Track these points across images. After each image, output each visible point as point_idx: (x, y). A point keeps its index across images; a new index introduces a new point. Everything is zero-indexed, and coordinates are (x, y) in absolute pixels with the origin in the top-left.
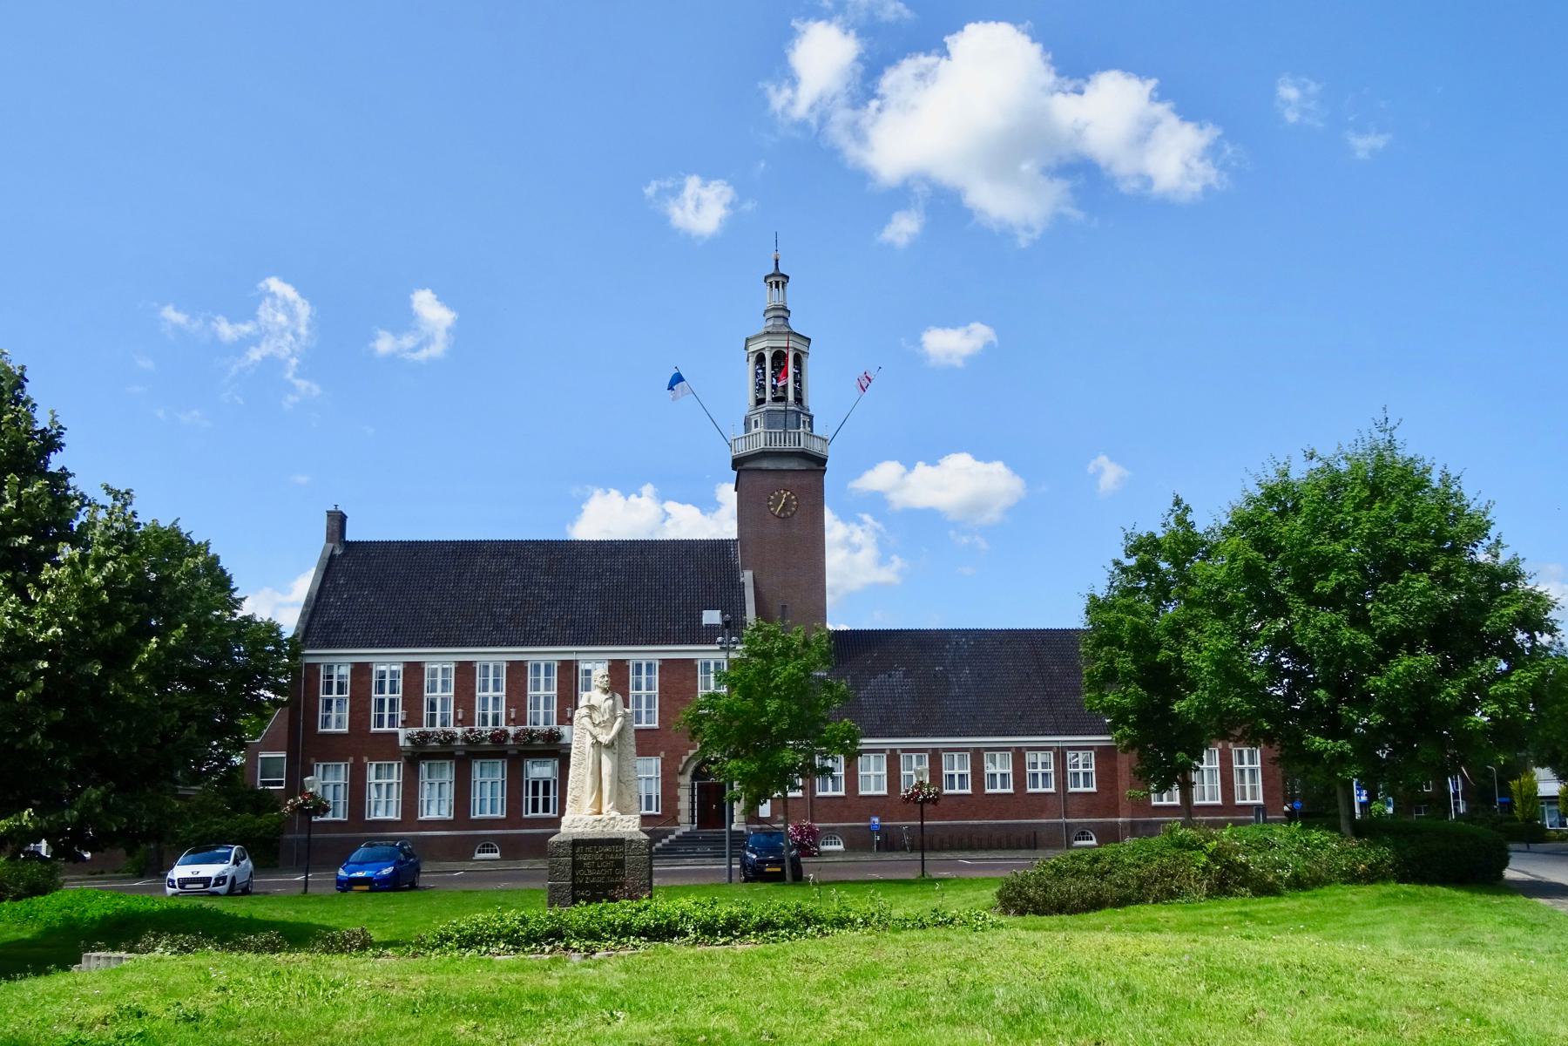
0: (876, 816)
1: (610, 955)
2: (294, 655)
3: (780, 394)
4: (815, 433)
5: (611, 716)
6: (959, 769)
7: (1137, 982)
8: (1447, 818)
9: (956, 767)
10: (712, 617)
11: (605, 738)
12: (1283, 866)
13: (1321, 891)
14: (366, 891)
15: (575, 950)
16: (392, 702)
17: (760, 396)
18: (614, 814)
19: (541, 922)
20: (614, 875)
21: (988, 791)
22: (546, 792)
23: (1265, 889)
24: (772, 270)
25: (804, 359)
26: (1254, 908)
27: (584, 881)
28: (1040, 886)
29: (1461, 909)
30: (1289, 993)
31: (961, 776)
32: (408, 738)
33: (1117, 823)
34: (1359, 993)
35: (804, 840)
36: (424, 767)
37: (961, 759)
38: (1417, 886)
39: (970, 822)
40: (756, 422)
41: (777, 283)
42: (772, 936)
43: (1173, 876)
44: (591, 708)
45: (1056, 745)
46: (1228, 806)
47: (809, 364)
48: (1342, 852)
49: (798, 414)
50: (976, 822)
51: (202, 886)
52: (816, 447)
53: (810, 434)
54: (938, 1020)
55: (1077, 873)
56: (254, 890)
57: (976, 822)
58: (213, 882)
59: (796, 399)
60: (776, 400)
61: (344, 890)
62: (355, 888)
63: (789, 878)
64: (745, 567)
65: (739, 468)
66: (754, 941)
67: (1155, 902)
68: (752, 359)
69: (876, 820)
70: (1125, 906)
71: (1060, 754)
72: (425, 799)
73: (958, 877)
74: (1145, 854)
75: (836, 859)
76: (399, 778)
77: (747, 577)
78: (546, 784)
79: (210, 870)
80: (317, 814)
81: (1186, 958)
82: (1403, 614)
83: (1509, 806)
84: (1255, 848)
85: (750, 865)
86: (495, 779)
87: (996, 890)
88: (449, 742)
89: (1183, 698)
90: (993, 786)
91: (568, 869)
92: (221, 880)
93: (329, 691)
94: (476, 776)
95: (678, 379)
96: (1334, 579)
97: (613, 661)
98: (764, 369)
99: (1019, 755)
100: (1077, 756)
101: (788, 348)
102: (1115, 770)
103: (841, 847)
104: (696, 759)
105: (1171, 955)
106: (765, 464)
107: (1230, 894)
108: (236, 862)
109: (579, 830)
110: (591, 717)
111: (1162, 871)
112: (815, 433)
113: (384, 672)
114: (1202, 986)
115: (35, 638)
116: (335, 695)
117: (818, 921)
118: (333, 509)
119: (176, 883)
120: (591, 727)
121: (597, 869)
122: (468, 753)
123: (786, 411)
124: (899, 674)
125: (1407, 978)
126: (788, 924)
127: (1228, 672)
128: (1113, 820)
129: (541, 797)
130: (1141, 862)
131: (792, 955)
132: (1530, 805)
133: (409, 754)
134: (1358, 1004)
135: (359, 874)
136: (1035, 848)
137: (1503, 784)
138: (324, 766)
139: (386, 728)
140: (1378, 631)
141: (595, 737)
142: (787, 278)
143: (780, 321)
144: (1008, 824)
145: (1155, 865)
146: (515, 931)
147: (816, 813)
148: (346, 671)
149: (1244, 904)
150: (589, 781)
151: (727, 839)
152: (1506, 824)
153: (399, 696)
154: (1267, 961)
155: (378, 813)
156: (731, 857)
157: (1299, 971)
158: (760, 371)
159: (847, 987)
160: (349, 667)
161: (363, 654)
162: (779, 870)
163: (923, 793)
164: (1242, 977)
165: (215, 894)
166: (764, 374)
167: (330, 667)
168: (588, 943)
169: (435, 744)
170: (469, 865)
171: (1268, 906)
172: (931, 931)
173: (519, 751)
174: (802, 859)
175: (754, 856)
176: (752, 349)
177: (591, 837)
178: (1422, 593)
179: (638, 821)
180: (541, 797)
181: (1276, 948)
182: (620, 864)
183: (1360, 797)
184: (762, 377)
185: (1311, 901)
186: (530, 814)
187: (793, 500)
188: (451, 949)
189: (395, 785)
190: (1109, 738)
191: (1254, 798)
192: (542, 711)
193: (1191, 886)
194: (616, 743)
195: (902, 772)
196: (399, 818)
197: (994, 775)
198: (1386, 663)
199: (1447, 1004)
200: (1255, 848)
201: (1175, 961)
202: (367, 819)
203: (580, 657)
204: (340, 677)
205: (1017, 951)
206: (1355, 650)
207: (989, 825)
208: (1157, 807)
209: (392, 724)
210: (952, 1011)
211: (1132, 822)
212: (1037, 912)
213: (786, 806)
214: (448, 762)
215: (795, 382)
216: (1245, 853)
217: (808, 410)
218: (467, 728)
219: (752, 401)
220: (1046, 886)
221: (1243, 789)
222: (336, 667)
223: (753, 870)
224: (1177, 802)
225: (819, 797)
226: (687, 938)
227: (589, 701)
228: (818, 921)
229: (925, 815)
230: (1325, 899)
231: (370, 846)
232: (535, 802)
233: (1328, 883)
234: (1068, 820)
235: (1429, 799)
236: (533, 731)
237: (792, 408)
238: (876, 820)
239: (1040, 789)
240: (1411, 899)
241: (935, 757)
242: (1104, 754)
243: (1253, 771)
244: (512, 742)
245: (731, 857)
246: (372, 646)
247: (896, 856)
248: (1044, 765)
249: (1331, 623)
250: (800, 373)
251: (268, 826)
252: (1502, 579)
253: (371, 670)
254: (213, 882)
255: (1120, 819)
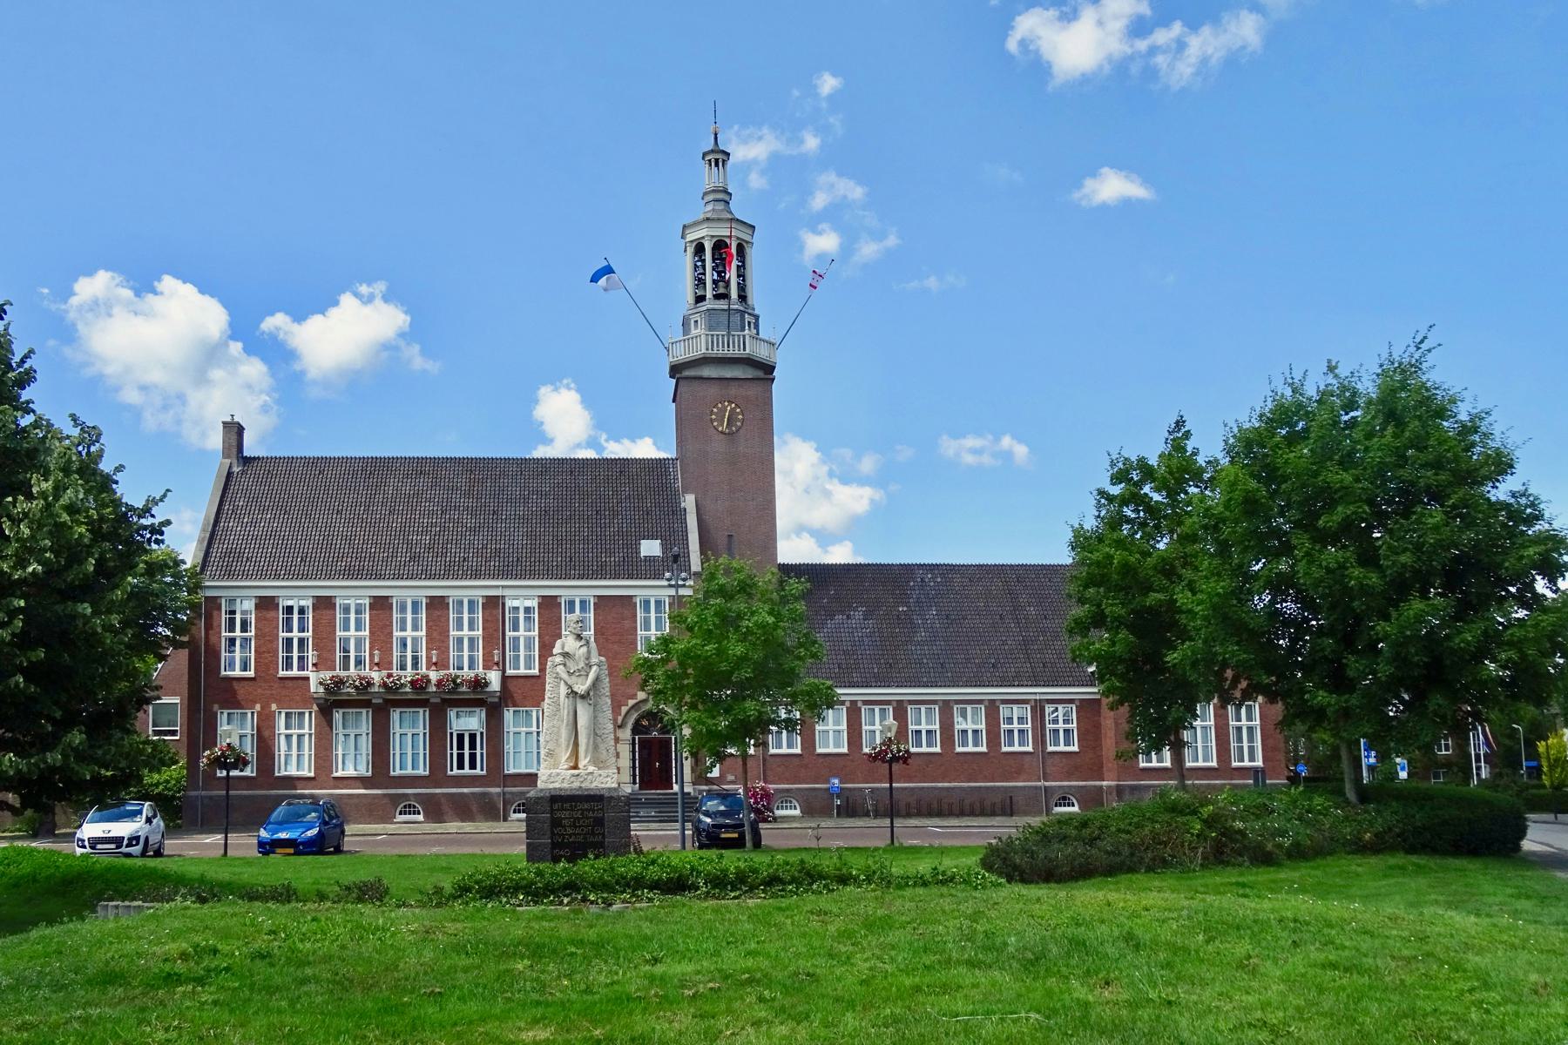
0: (835, 776)
1: (627, 907)
2: (195, 588)
3: (722, 290)
4: (761, 336)
5: (587, 665)
6: (927, 724)
7: (1139, 932)
8: (1469, 785)
9: (925, 722)
10: (651, 548)
11: (581, 688)
12: (1283, 833)
13: (1324, 862)
14: (289, 854)
15: (592, 902)
16: (301, 641)
17: (700, 293)
18: (591, 769)
19: (558, 875)
20: (593, 834)
21: (959, 749)
22: (473, 746)
23: (1264, 858)
24: (711, 146)
25: (748, 250)
26: (1252, 878)
27: (564, 838)
28: (1027, 852)
29: (1472, 881)
30: (1282, 942)
31: (929, 732)
32: (321, 683)
33: (1101, 787)
34: (1347, 944)
35: (758, 803)
36: (338, 716)
37: (929, 711)
38: (1427, 858)
39: (940, 785)
40: (696, 322)
41: (717, 161)
42: (780, 890)
43: (1165, 844)
44: (566, 655)
45: (1033, 697)
46: (1224, 770)
47: (753, 255)
48: (1346, 818)
49: (742, 313)
50: (946, 785)
51: (113, 846)
52: (762, 352)
53: (756, 337)
54: (958, 962)
55: (1064, 839)
56: (165, 853)
57: (946, 785)
58: (125, 842)
59: (740, 296)
60: (717, 297)
61: (265, 853)
62: (278, 850)
63: (749, 844)
64: (686, 490)
65: (678, 376)
66: (763, 895)
67: (1146, 872)
68: (691, 250)
69: (836, 781)
70: (1116, 875)
71: (1038, 708)
72: (340, 752)
73: (931, 846)
74: (1135, 820)
75: (794, 825)
76: (310, 729)
77: (689, 502)
78: (473, 737)
79: (122, 829)
80: (154, 769)
81: (1185, 913)
82: (1414, 553)
83: (1536, 772)
84: (1253, 814)
85: (704, 830)
86: (415, 731)
87: (981, 856)
88: (366, 688)
89: (1175, 649)
90: (965, 744)
91: (547, 826)
92: (134, 840)
93: (232, 628)
94: (396, 728)
95: (608, 270)
96: (1341, 511)
97: (317, 598)
98: (703, 261)
99: (992, 708)
100: (1057, 710)
101: (730, 237)
102: (1098, 726)
103: (797, 812)
104: (636, 711)
105: (1170, 910)
106: (707, 372)
107: (1226, 864)
108: (149, 821)
109: (557, 785)
110: (565, 665)
111: (1155, 837)
112: (761, 336)
113: (292, 607)
114: (1201, 936)
115: (11, 575)
116: (238, 633)
117: (821, 877)
118: (228, 419)
119: (86, 843)
120: (565, 676)
121: (576, 827)
122: (387, 701)
123: (729, 309)
124: (858, 615)
125: (1395, 932)
126: (793, 880)
127: (1225, 618)
128: (1098, 783)
129: (467, 752)
130: (1130, 828)
131: (805, 909)
132: (1559, 770)
133: (322, 701)
134: (1347, 953)
135: (283, 835)
136: (1012, 815)
137: (1531, 745)
138: (229, 714)
139: (295, 672)
140: (1389, 572)
141: (570, 687)
142: (728, 154)
143: (720, 206)
144: (980, 787)
145: (1147, 831)
146: (533, 883)
147: (769, 773)
148: (249, 605)
149: (1241, 874)
150: (564, 733)
151: (679, 801)
152: (1534, 791)
153: (309, 634)
154: (1261, 916)
155: (289, 767)
156: (684, 821)
157: (1292, 925)
158: (699, 264)
159: (866, 936)
160: (253, 601)
161: (269, 587)
162: (736, 835)
163: (892, 751)
164: (1238, 929)
165: (128, 855)
166: (704, 269)
167: (232, 601)
168: (605, 895)
169: (349, 690)
170: (390, 828)
171: (1266, 877)
172: (935, 890)
173: (384, 699)
174: (761, 825)
175: (708, 820)
176: (690, 237)
177: (568, 793)
178: (1436, 528)
179: (539, 782)
180: (467, 752)
181: (1270, 906)
182: (599, 822)
183: (1369, 759)
184: (701, 271)
185: (1313, 872)
186: (456, 771)
187: (738, 414)
188: (474, 899)
189: (307, 737)
190: (1095, 690)
191: (1252, 759)
192: (466, 653)
193: (1185, 854)
194: (591, 694)
195: (864, 727)
196: (254, 775)
197: (965, 732)
198: (1396, 607)
199: (1429, 954)
200: (1253, 814)
201: (1175, 915)
202: (277, 774)
203: (506, 592)
204: (243, 612)
205: (1021, 905)
206: (1364, 590)
207: (961, 788)
208: (1145, 769)
209: (301, 668)
210: (970, 955)
211: (1118, 786)
212: (1024, 881)
213: (745, 764)
214: (364, 711)
215: (739, 276)
216: (1242, 819)
217: (754, 309)
218: (442, 673)
219: (691, 299)
220: (1033, 852)
221: (1241, 749)
222: (238, 601)
223: (709, 836)
224: (1167, 764)
225: (819, 755)
226: (699, 892)
227: (563, 648)
228: (821, 877)
229: (894, 777)
230: (1327, 869)
231: (289, 804)
232: (461, 757)
233: (1331, 853)
234: (1047, 784)
235: (1447, 764)
236: (457, 677)
237: (737, 306)
238: (836, 781)
239: (1017, 748)
240: (1419, 870)
241: (900, 710)
242: (1087, 709)
243: (1250, 729)
244: (434, 689)
245: (684, 821)
246: (277, 577)
247: (859, 822)
248: (1021, 720)
249: (1337, 562)
250: (744, 266)
251: (167, 782)
252: (1522, 513)
253: (278, 604)
254: (125, 842)
255: (1105, 783)
